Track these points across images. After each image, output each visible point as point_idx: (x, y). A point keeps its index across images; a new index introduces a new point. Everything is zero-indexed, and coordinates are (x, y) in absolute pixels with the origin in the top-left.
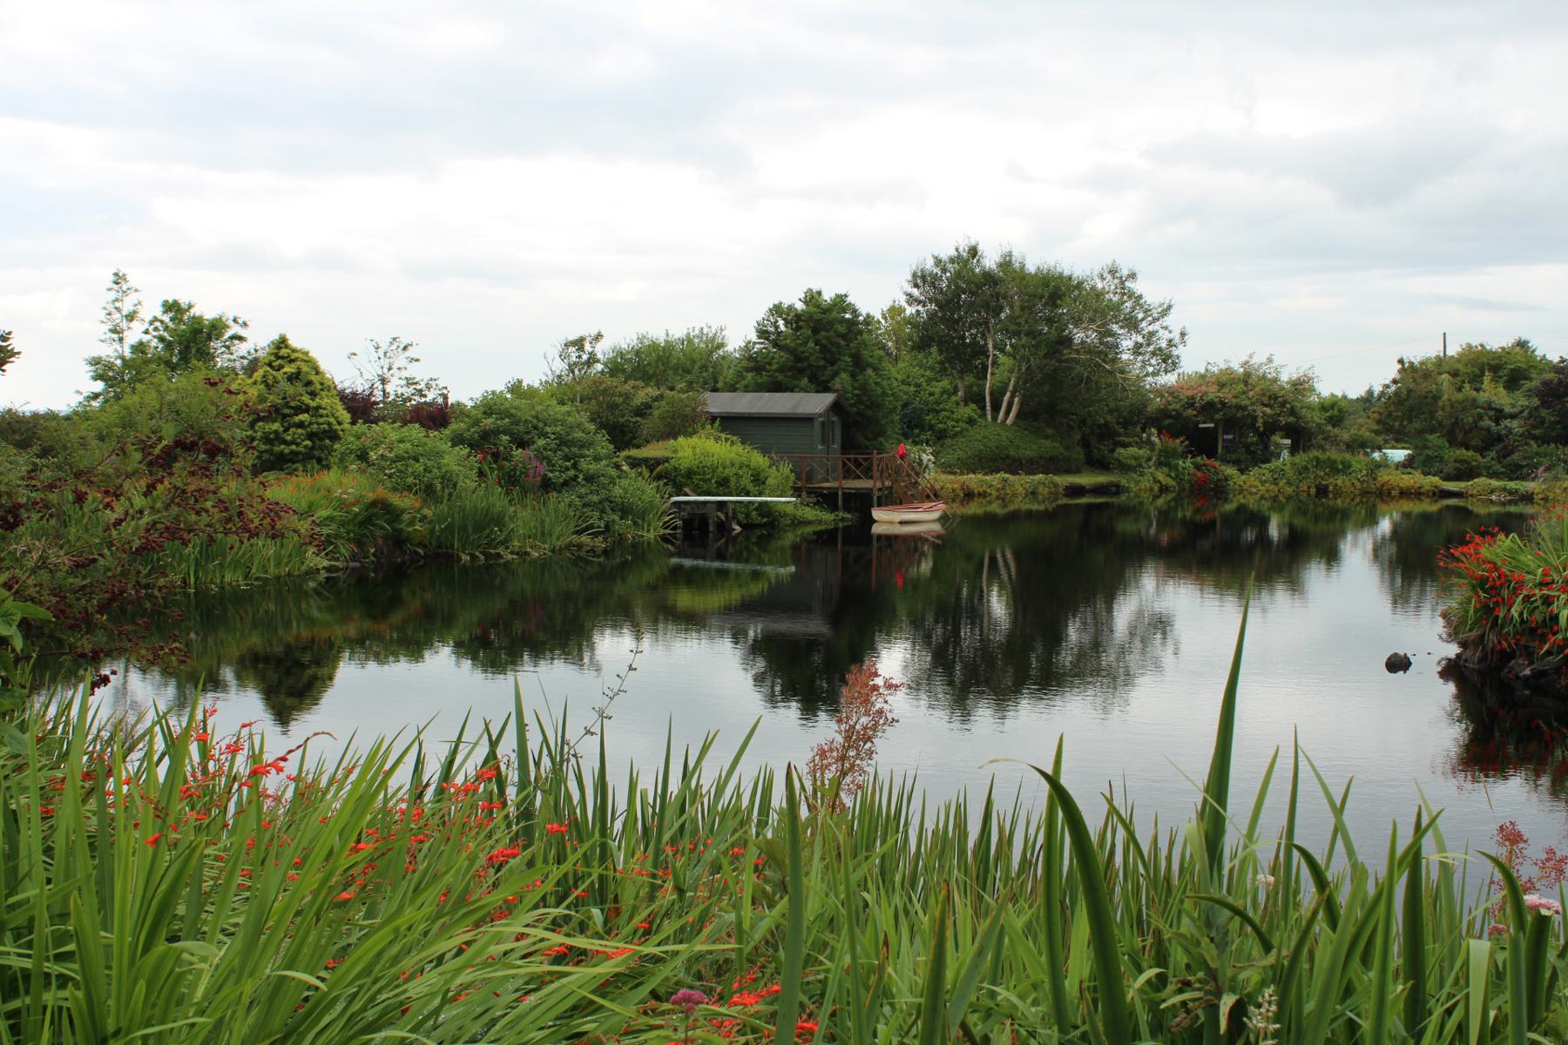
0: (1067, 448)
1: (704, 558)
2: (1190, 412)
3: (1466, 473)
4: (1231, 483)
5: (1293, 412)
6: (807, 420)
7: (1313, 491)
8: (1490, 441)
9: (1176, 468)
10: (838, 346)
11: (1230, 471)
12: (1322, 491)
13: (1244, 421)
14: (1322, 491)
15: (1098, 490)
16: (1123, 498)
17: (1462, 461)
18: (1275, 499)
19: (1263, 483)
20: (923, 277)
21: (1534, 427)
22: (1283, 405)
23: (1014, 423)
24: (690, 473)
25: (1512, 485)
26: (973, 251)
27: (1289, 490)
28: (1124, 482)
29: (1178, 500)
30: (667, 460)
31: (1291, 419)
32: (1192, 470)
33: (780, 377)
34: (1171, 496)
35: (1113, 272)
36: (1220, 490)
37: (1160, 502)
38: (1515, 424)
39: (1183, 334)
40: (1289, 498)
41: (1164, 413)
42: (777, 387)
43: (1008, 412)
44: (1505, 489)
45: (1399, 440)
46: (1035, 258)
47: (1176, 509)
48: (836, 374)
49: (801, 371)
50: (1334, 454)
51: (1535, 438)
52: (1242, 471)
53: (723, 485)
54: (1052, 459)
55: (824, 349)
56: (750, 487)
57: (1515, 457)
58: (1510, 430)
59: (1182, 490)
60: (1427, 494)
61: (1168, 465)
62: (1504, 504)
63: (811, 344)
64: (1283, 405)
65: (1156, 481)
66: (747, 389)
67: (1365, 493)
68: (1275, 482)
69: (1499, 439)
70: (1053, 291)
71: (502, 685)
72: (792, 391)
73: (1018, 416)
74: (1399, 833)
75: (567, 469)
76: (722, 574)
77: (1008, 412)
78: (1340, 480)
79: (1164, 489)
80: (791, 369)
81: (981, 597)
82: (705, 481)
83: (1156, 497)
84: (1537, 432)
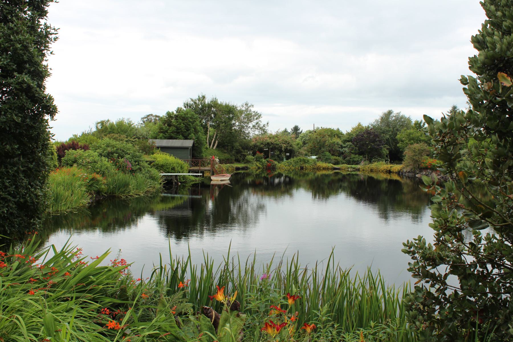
0: (231, 156)
1: (171, 193)
2: (262, 146)
3: (337, 163)
4: (275, 165)
5: (291, 146)
6: (186, 148)
7: (299, 168)
8: (341, 154)
9: (262, 162)
10: (190, 125)
11: (276, 163)
12: (302, 168)
13: (275, 149)
14: (302, 168)
15: (243, 169)
16: (248, 171)
17: (336, 160)
18: (289, 170)
19: (286, 166)
20: (187, 105)
21: (352, 150)
22: (288, 144)
23: (216, 149)
24: (162, 166)
25: (353, 166)
26: (204, 97)
27: (293, 168)
28: (248, 166)
29: (262, 171)
30: (154, 162)
31: (291, 148)
32: (266, 162)
33: (172, 135)
34: (261, 170)
35: (246, 104)
36: (274, 168)
37: (258, 172)
38: (346, 149)
39: (268, 124)
40: (293, 170)
41: (255, 146)
42: (171, 138)
43: (213, 146)
44: (351, 167)
45: (312, 154)
46: (222, 100)
47: (262, 174)
48: (190, 134)
49: (178, 133)
50: (302, 158)
51: (352, 153)
52: (279, 163)
53: (173, 170)
54: (228, 159)
55: (186, 126)
56: (180, 170)
57: (348, 158)
58: (345, 151)
59: (264, 168)
60: (330, 169)
61: (259, 161)
62: (351, 171)
63: (182, 124)
64: (288, 144)
65: (257, 166)
66: (161, 138)
67: (314, 169)
68: (289, 166)
69: (342, 153)
70: (230, 111)
71: (183, 243)
72: (176, 139)
73: (217, 147)
74: (256, 258)
75: (136, 165)
76: (173, 198)
77: (213, 146)
78: (307, 165)
79: (259, 168)
80: (176, 132)
81: (206, 202)
82: (167, 168)
83: (257, 170)
84: (353, 151)
